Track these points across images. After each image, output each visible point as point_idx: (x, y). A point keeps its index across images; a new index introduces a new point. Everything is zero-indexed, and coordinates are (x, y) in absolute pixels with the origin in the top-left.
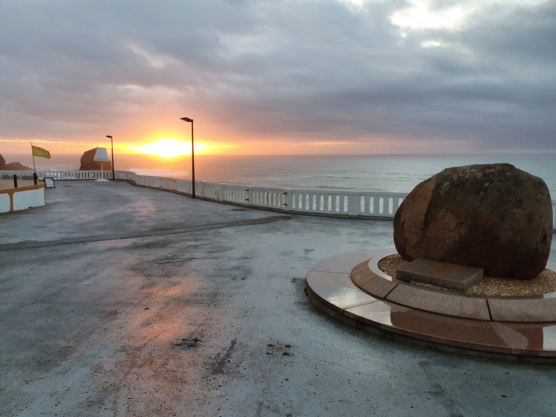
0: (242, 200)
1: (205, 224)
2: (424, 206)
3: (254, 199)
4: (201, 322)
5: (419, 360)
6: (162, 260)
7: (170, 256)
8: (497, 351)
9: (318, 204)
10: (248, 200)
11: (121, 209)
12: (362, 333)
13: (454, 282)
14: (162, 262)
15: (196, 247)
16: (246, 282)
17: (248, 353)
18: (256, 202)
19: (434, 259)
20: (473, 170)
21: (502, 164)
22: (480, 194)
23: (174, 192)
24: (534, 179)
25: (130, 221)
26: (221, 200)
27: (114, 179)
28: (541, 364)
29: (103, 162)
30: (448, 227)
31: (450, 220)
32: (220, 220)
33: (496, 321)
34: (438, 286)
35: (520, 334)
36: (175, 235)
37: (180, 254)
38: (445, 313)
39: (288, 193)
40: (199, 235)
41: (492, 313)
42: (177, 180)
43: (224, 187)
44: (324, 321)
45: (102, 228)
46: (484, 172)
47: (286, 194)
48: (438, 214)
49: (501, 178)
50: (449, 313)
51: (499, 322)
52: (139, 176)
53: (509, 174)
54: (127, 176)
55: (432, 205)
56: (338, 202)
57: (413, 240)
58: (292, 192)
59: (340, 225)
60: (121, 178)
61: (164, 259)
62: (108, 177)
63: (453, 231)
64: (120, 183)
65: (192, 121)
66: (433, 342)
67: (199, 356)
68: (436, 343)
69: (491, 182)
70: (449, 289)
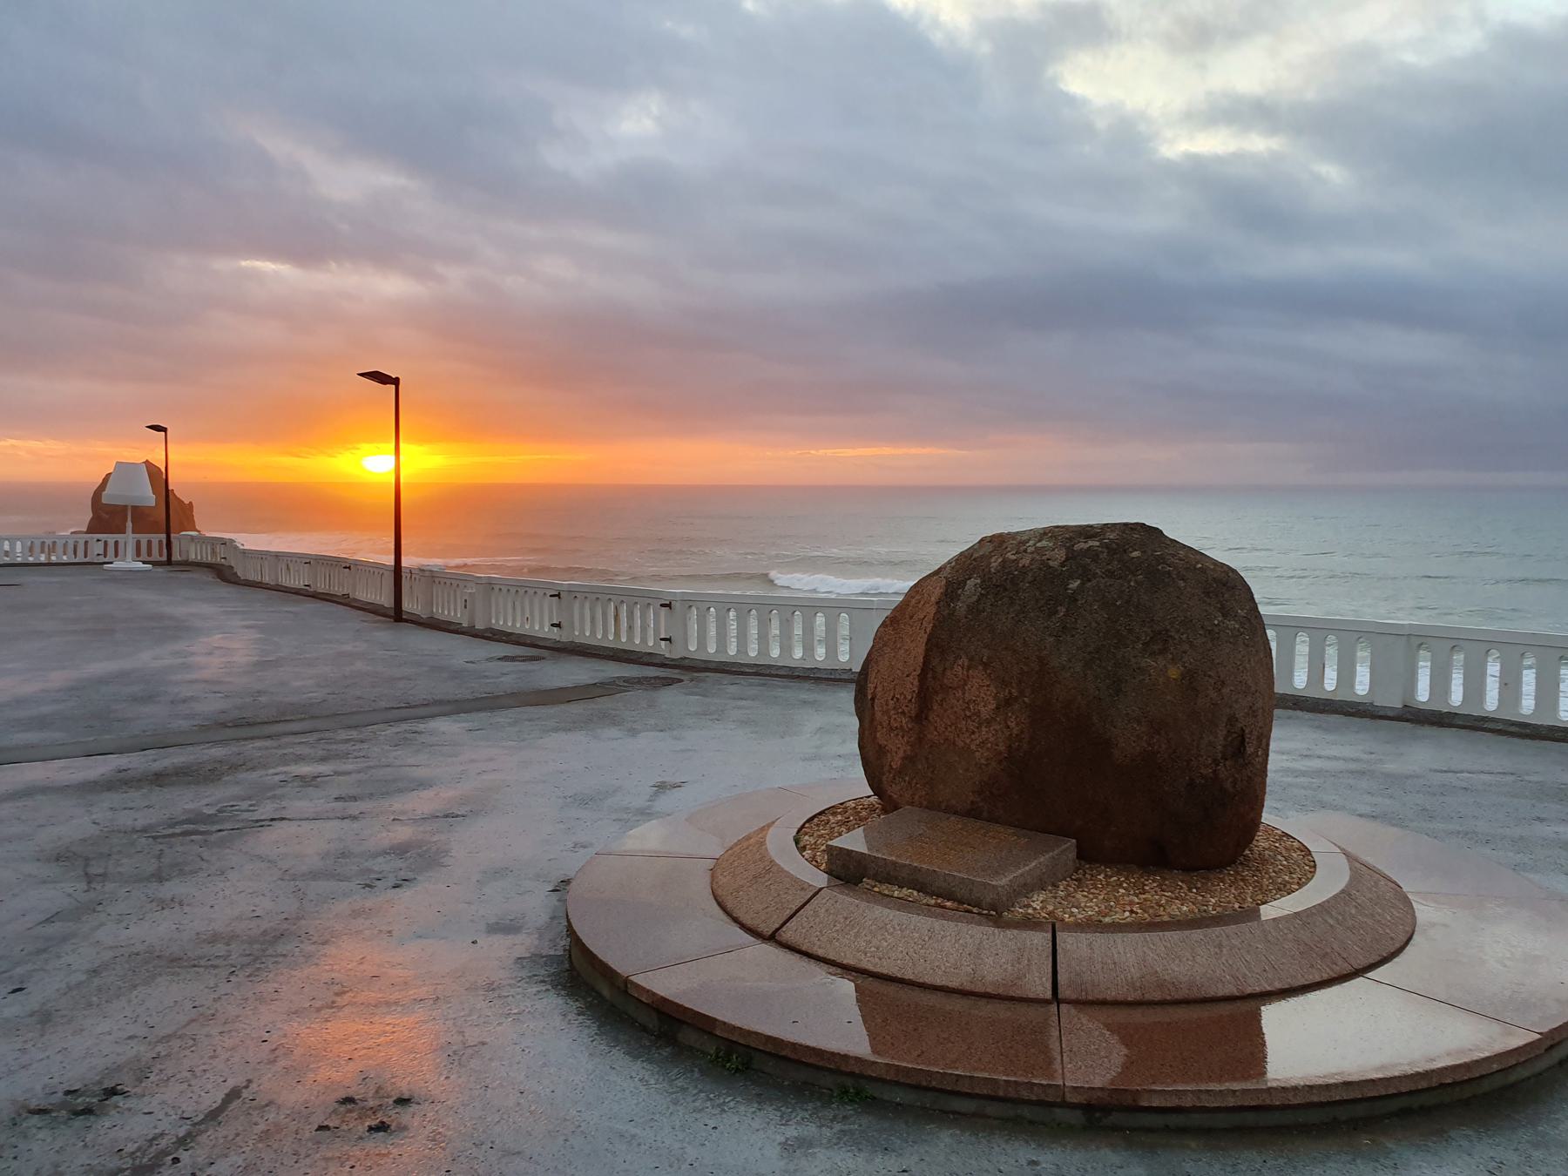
0: (542, 626)
2: (916, 649)
3: (577, 624)
5: (792, 1132)
7: (211, 811)
8: (1025, 1094)
9: (763, 638)
10: (558, 625)
11: (148, 658)
12: (666, 1052)
13: (973, 882)
14: (170, 831)
16: (406, 894)
18: (586, 631)
19: (950, 810)
20: (1044, 543)
21: (1126, 524)
22: (1056, 612)
23: (346, 602)
24: (1203, 571)
25: (149, 698)
26: (479, 626)
27: (169, 562)
28: (1150, 1130)
29: (135, 508)
30: (978, 714)
31: (981, 693)
33: (1068, 1002)
34: (931, 894)
36: (268, 743)
37: (245, 805)
38: (928, 980)
40: (347, 741)
41: (1062, 978)
43: (490, 585)
44: (571, 1016)
45: (42, 723)
46: (1070, 549)
47: (669, 606)
48: (948, 673)
50: (938, 982)
52: (244, 552)
53: (1135, 554)
55: (935, 646)
58: (689, 602)
59: (812, 704)
60: (192, 557)
61: (188, 821)
62: (149, 554)
63: (989, 722)
65: (396, 382)
66: (852, 1074)
67: (85, 1146)
68: (861, 1076)
69: (1086, 576)
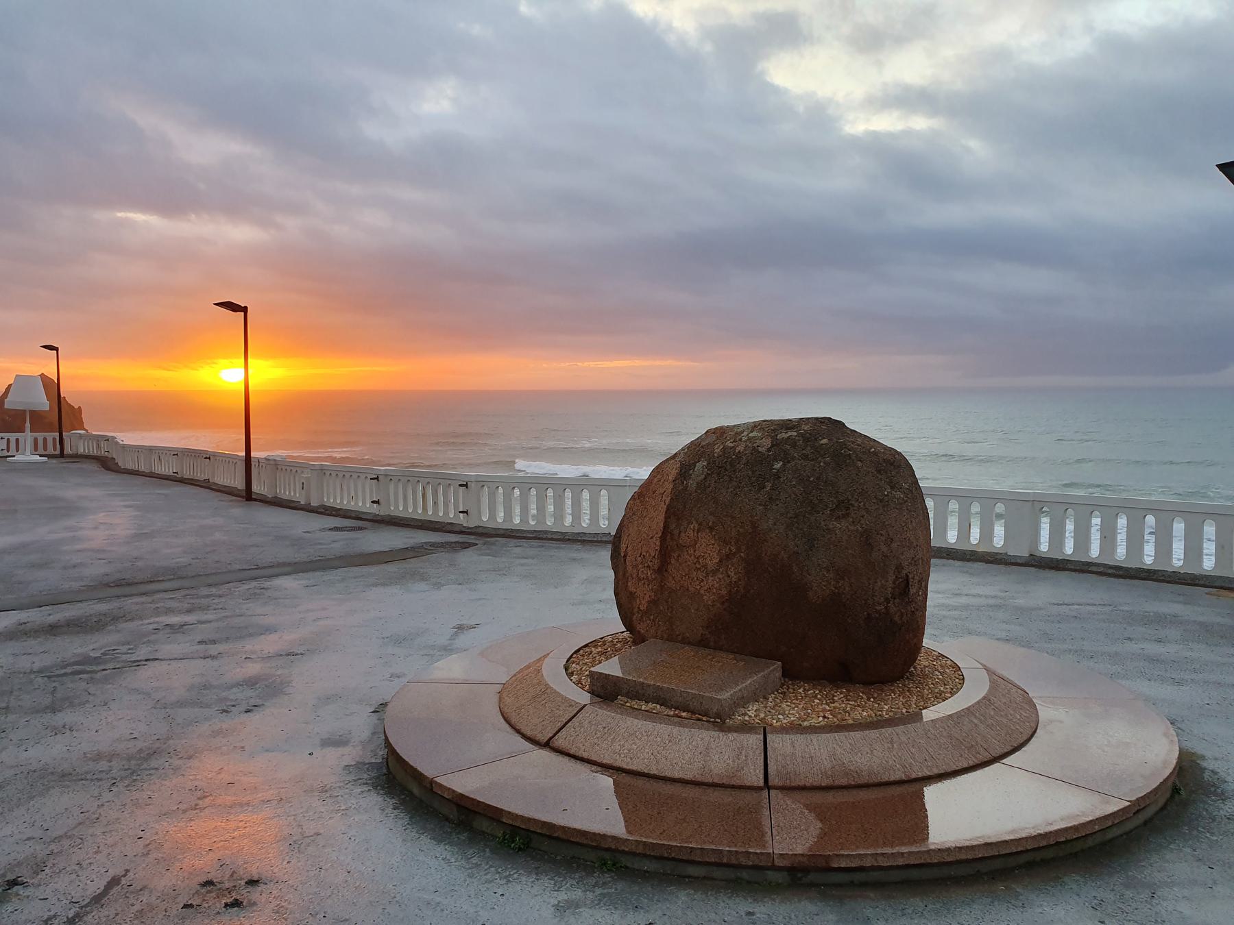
0: (364, 503)
1: (238, 567)
2: (656, 517)
4: (60, 833)
6: (65, 667)
8: (744, 861)
10: (377, 502)
11: (44, 532)
12: (464, 836)
14: (63, 671)
15: (179, 629)
16: (256, 717)
17: (136, 908)
19: (685, 641)
20: (754, 434)
23: (207, 485)
26: (314, 503)
30: (705, 566)
31: (708, 549)
32: (287, 554)
35: (812, 817)
36: (144, 599)
37: (124, 649)
38: (668, 774)
39: (472, 485)
42: (215, 455)
43: (322, 470)
46: (774, 438)
47: (466, 485)
49: (808, 451)
50: (676, 775)
51: (782, 788)
52: (124, 447)
53: (824, 441)
54: (98, 447)
55: (670, 513)
56: (586, 505)
57: (644, 594)
58: (481, 483)
60: (81, 451)
62: (45, 448)
63: (714, 572)
64: (78, 465)
65: (245, 310)
66: (608, 850)
68: (616, 851)
69: (787, 459)
70: (693, 713)
